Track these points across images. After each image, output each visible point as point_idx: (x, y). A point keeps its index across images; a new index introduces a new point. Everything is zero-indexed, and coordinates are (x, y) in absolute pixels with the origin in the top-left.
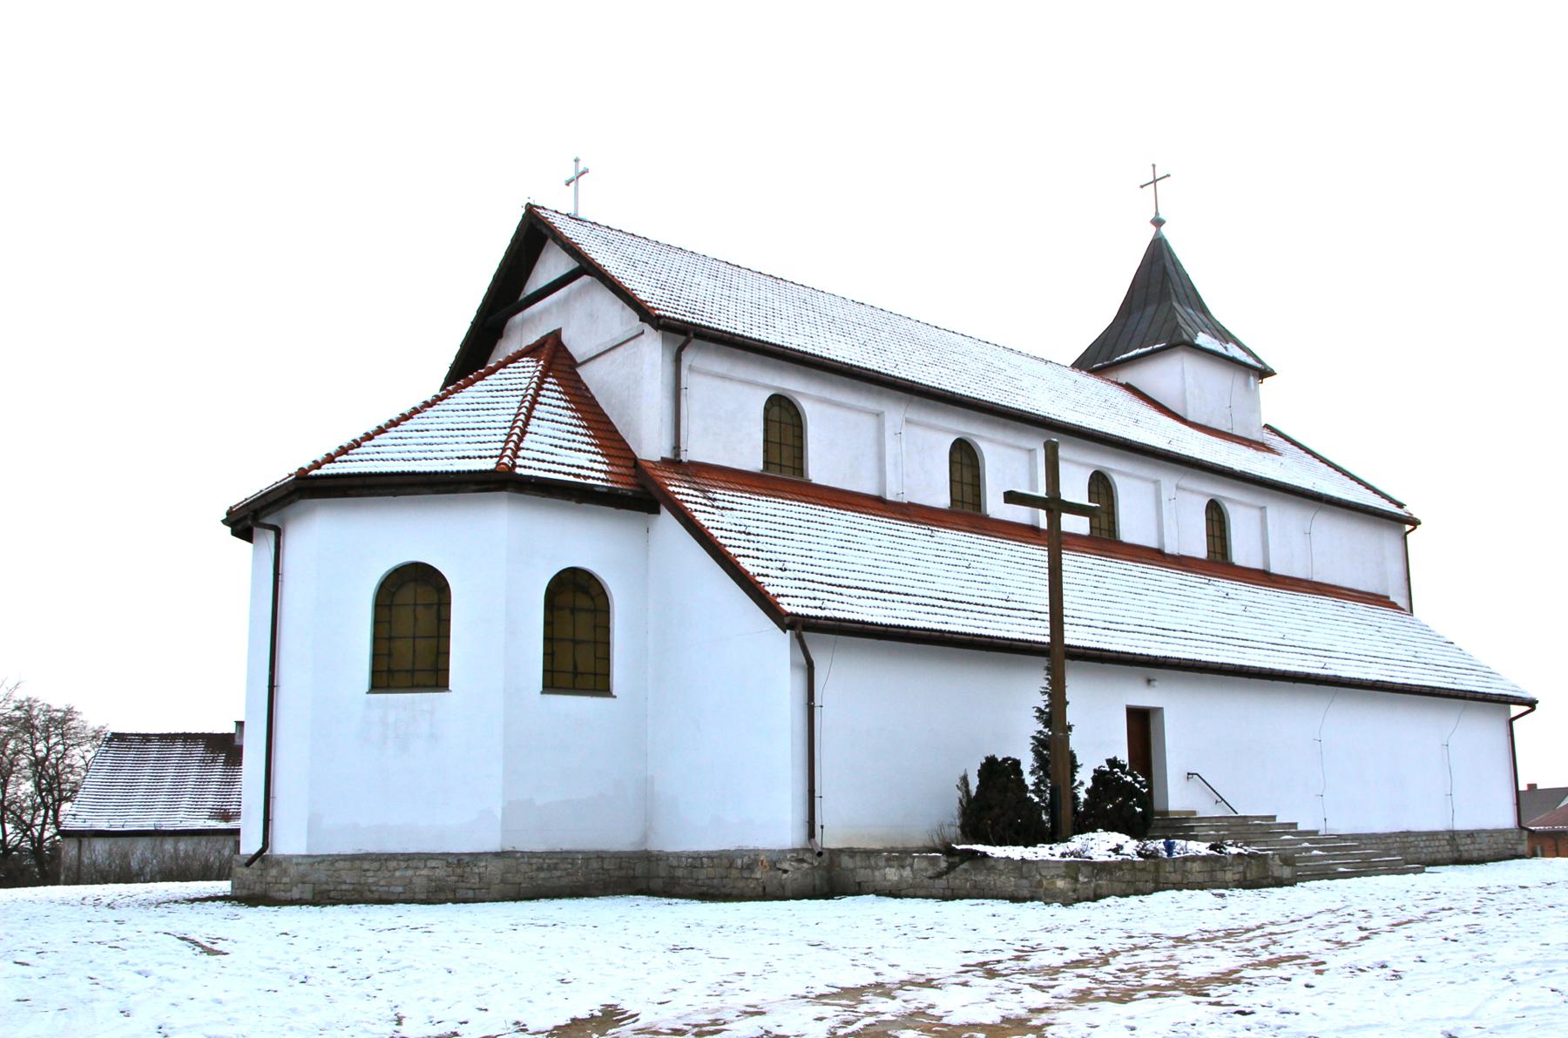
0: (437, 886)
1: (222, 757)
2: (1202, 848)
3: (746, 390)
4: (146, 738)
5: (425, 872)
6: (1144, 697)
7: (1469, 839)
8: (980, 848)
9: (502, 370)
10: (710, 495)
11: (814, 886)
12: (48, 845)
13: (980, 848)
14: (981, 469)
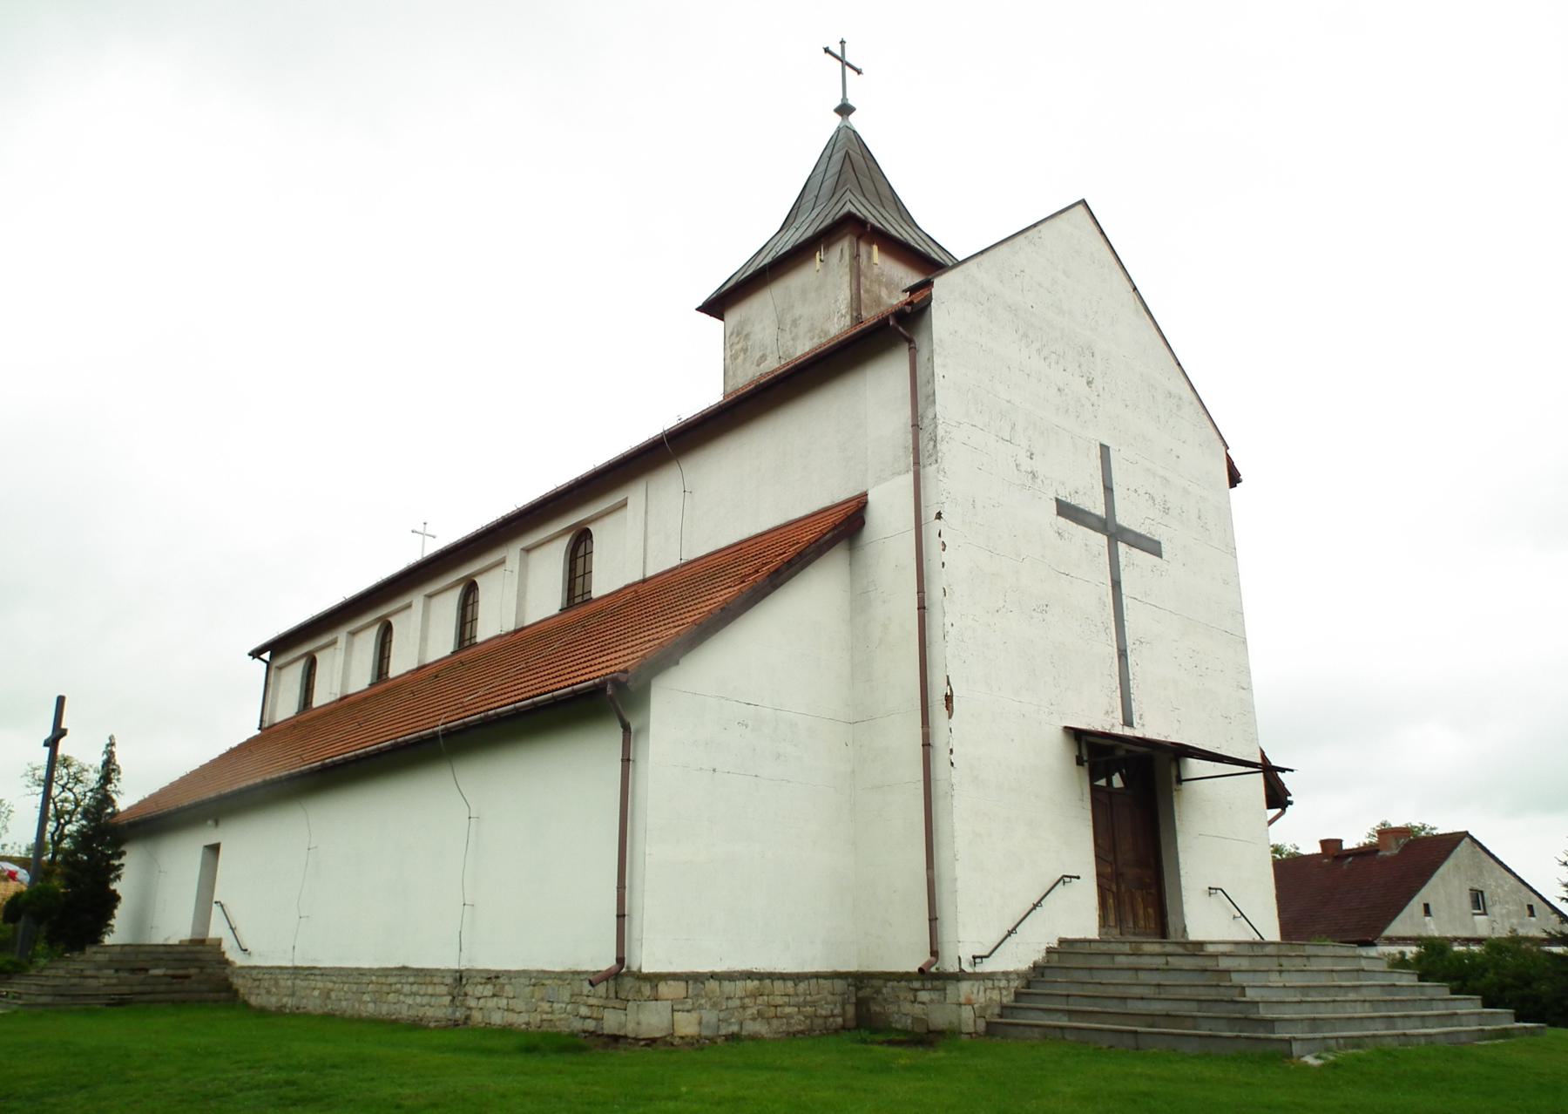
11: (345, 1011)
12: (67, 846)
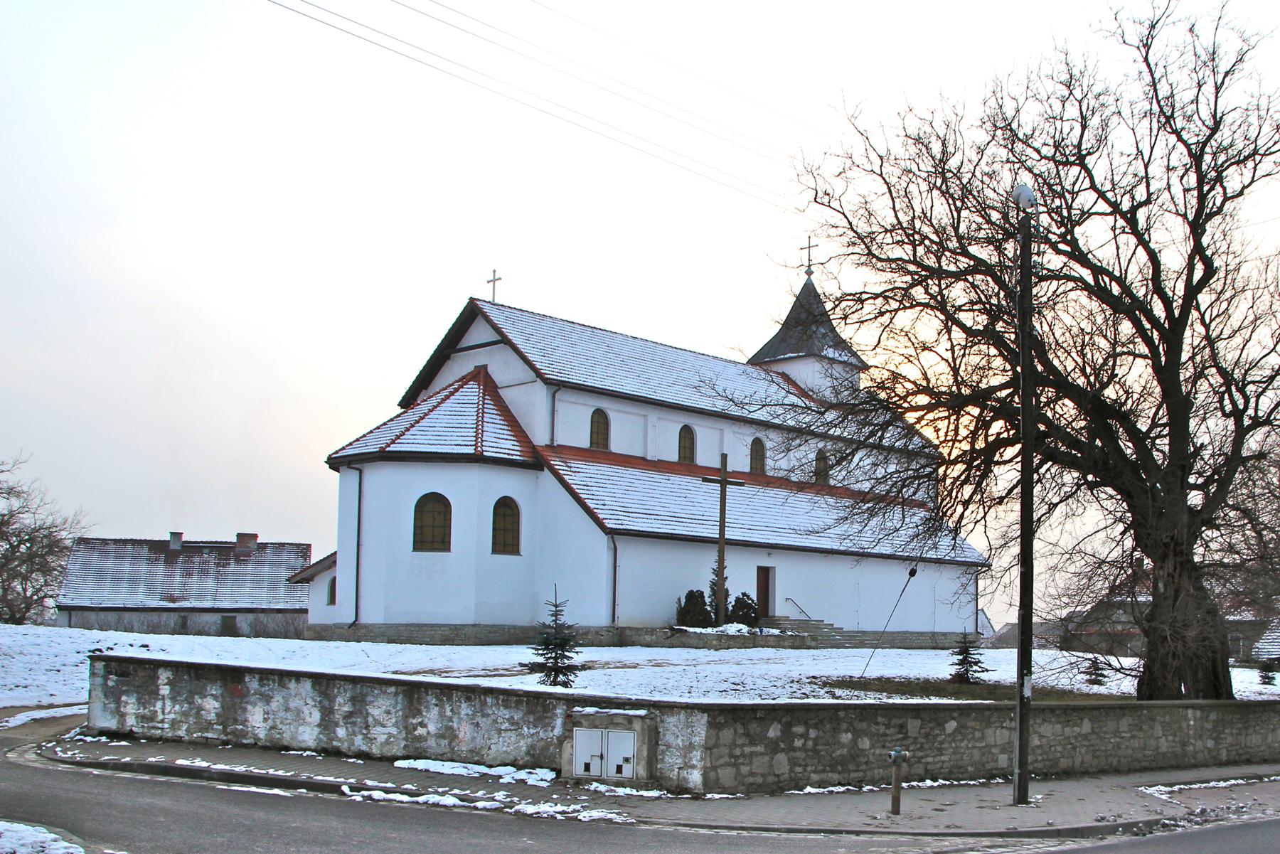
1: (163, 557)
2: (776, 632)
3: (582, 408)
4: (104, 542)
6: (766, 562)
8: (684, 628)
9: (461, 390)
10: (569, 465)
13: (684, 628)
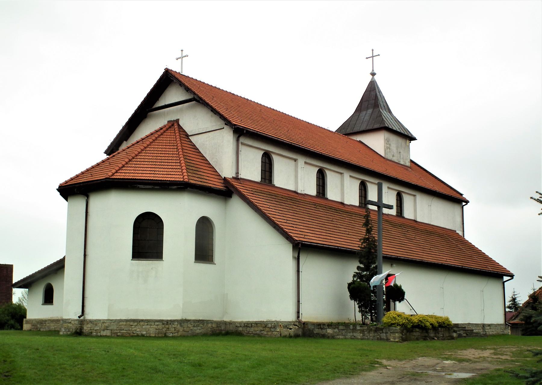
0: (158, 332)
5: (154, 326)
7: (489, 327)
14: (402, 211)
